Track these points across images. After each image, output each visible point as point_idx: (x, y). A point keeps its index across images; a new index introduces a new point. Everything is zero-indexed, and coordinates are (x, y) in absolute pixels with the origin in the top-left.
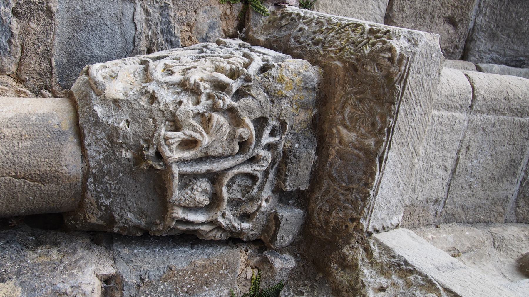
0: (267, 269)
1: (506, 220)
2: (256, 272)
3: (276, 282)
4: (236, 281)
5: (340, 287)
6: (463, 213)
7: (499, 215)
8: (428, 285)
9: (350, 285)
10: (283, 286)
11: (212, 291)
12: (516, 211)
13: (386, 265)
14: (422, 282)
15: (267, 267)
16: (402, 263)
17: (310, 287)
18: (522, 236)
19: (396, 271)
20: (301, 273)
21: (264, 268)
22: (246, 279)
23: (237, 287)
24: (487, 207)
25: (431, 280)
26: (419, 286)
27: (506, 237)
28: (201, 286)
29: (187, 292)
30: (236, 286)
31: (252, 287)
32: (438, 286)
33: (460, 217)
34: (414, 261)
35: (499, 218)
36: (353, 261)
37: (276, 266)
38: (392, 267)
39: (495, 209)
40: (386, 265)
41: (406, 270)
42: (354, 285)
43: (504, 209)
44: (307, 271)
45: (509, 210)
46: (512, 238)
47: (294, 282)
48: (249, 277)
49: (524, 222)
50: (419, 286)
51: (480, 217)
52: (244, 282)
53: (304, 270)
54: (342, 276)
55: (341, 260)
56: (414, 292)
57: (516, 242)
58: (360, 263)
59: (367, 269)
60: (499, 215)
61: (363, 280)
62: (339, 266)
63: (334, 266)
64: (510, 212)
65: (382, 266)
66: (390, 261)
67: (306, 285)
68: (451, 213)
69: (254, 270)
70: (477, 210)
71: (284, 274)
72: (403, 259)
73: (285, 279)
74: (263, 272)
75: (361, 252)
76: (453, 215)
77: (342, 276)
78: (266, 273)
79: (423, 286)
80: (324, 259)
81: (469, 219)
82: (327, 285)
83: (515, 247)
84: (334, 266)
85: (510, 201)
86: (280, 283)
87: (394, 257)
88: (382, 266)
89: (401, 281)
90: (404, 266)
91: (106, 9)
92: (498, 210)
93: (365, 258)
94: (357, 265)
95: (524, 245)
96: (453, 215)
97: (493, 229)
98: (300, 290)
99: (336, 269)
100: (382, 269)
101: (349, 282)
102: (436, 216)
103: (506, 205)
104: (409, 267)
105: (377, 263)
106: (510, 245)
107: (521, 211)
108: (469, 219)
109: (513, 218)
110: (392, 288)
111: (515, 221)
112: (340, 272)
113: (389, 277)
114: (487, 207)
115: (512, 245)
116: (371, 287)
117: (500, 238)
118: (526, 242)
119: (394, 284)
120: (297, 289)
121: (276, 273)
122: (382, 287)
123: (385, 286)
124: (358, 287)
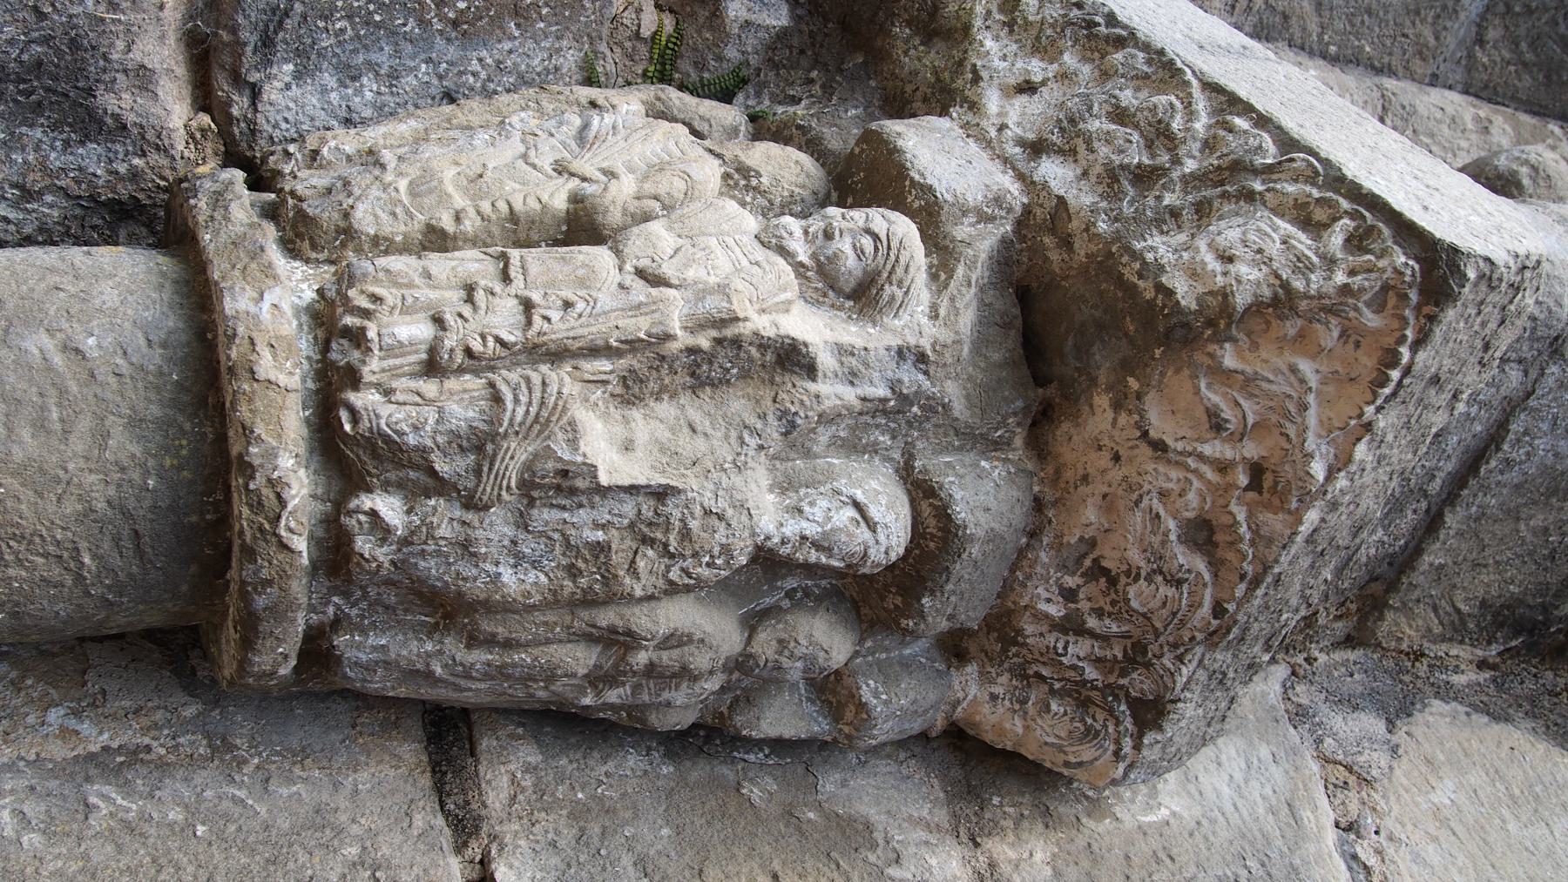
0: (701, 20)
1: (1435, 76)
2: (669, 23)
3: (725, 66)
4: (605, 32)
5: (909, 88)
6: (1316, 19)
7: (1420, 53)
8: (1161, 73)
9: (938, 80)
10: (745, 81)
11: (530, 44)
12: (1471, 56)
13: (1052, 26)
14: (1145, 68)
15: (703, 13)
16: (1098, 19)
17: (823, 87)
18: (1468, 118)
19: (1076, 41)
20: (802, 52)
21: (693, 14)
22: (637, 35)
23: (608, 53)
24: (1390, 17)
25: (1171, 62)
26: (1136, 77)
27: (1421, 109)
28: (499, 16)
29: (455, 24)
30: (603, 47)
31: (652, 69)
32: (1189, 76)
33: (1304, 29)
34: (1136, 19)
35: (1417, 66)
36: (958, 18)
37: (731, 14)
38: (1068, 32)
39: (1410, 32)
40: (1052, 26)
41: (1107, 39)
42: (948, 80)
43: (1437, 38)
44: (822, 46)
45: (1452, 47)
46: (1439, 115)
47: (778, 75)
48: (646, 32)
49: (1484, 94)
50: (1136, 77)
51: (1362, 48)
52: (628, 44)
53: (813, 45)
54: (919, 59)
55: (924, 15)
56: (1117, 92)
57: (1446, 130)
58: (978, 23)
59: (997, 38)
60: (1420, 53)
61: (979, 64)
62: (916, 32)
63: (900, 31)
64: (1454, 53)
65: (1041, 30)
66: (1066, 15)
68: (1280, 8)
69: (663, 16)
70: (1358, 21)
71: (751, 43)
72: (1106, 10)
73: (754, 60)
74: (690, 30)
76: (1286, 17)
77: (919, 59)
78: (699, 33)
79: (1146, 77)
80: (876, 14)
81: (1328, 44)
82: (873, 83)
83: (1439, 144)
85: (1462, 16)
86: (735, 72)
88: (1041, 30)
89: (1086, 70)
90: (1103, 29)
92: (1418, 36)
93: (995, 10)
94: (967, 28)
95: (1464, 144)
96: (1286, 17)
97: (1390, 83)
99: (907, 41)
100: (1038, 38)
101: (935, 72)
102: (1233, 7)
103: (1449, 24)
104: (1118, 31)
105: (1027, 23)
106: (1426, 134)
107: (1485, 60)
108: (1328, 44)
109: (1458, 76)
110: (1055, 86)
111: (1460, 87)
112: (915, 48)
114: (1390, 17)
115: (1432, 135)
116: (996, 81)
117: (1404, 107)
118: (1474, 137)
119: (1064, 76)
120: (783, 91)
121: (728, 35)
122: (1027, 82)
123: (1037, 78)
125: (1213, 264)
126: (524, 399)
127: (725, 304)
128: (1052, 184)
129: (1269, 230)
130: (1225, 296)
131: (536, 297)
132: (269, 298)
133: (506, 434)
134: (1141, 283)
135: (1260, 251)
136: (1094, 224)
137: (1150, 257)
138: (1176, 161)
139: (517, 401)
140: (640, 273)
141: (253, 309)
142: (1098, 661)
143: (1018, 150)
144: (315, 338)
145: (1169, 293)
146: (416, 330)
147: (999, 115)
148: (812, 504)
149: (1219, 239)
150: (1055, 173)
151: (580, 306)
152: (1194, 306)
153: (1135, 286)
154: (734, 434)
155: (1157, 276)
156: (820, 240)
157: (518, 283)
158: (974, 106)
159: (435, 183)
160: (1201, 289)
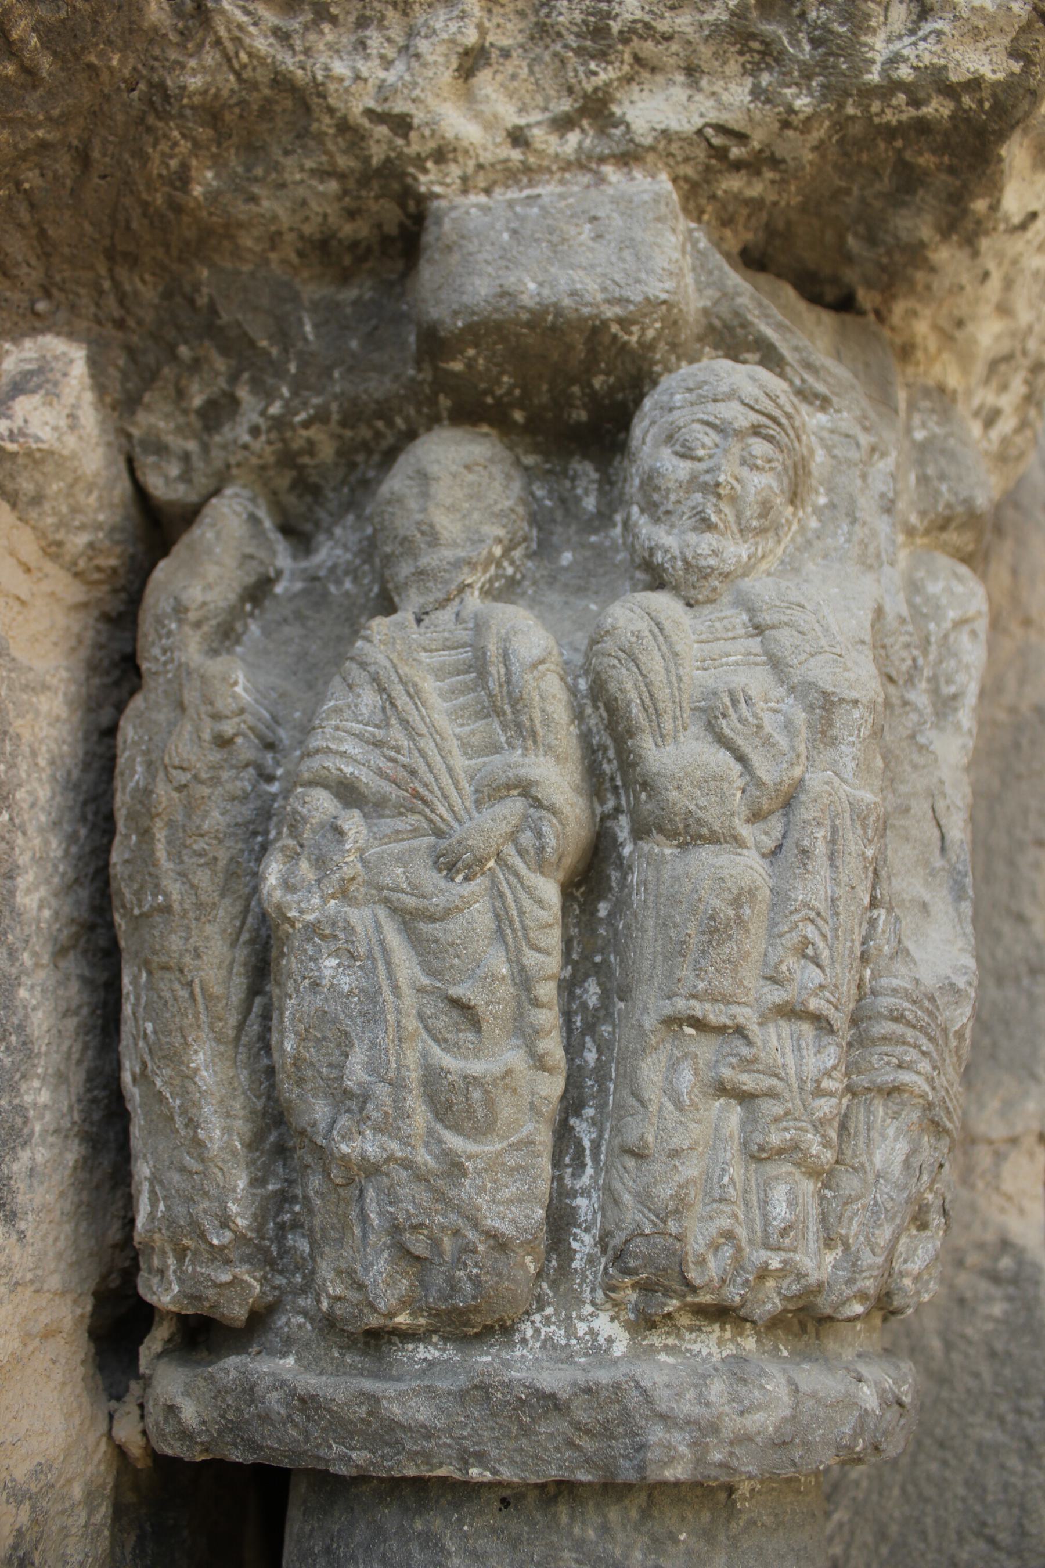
58: (288, 62)
94: (281, 82)
98: (197, 401)
122: (467, 53)
126: (912, 1055)
134: (927, 110)
136: (791, 110)
137: (904, 73)
142: (157, 1423)
143: (573, 138)
144: (691, 1329)
145: (975, 84)
157: (746, 1015)
160: (1004, 41)
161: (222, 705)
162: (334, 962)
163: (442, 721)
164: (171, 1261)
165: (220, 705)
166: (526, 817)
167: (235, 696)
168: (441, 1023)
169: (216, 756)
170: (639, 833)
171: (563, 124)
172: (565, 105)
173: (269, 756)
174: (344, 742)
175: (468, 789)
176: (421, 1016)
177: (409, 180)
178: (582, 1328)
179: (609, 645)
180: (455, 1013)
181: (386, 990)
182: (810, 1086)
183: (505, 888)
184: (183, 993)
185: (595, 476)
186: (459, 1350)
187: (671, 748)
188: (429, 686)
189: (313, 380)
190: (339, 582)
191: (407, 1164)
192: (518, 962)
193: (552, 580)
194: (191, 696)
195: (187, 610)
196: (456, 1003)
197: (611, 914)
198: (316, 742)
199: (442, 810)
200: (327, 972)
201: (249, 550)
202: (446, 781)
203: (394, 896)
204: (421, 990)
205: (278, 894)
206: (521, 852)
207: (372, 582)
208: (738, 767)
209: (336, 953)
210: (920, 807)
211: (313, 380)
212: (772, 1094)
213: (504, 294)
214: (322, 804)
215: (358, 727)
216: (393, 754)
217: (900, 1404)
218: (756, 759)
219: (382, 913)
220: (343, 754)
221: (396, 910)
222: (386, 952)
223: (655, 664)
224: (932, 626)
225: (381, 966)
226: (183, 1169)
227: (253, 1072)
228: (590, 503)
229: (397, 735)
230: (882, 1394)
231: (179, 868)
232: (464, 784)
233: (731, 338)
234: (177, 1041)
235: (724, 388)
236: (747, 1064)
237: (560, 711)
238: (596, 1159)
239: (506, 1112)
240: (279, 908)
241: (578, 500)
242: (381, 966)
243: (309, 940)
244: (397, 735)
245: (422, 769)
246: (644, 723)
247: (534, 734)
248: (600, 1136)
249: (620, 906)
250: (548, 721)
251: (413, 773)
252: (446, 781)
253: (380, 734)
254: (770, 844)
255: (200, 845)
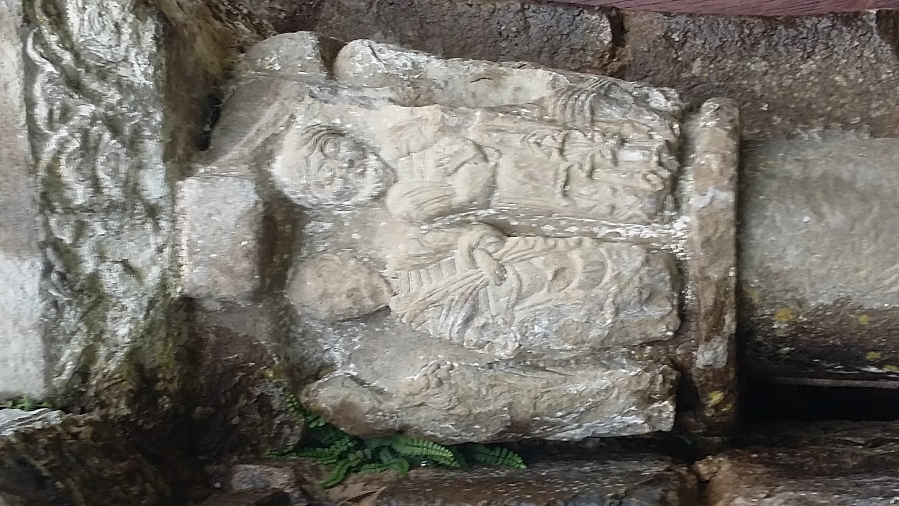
16: (54, 277)
40: (80, 304)
42: (163, 327)
58: (120, 355)
61: (141, 316)
63: (166, 403)
65: (90, 309)
67: (241, 414)
75: (99, 376)
84: (166, 403)
87: (55, 303)
91: (805, 41)
98: (258, 416)
113: (95, 278)
124: (161, 317)
125: (126, 31)
127: (446, 117)
128: (162, 176)
129: (86, 23)
130: (134, 10)
131: (556, 155)
132: (707, 199)
133: (593, 92)
135: (101, 15)
138: (94, 118)
139: (583, 103)
140: (486, 159)
141: (717, 192)
143: (163, 224)
146: (629, 156)
147: (154, 263)
148: (405, 65)
149: (113, 43)
150: (153, 184)
151: (532, 140)
152: (150, 20)
153: (166, 65)
154: (450, 88)
155: (156, 55)
156: (357, 163)
157: (563, 166)
158: (163, 285)
159: (589, 269)
161: (423, 384)
162: (536, 327)
163: (442, 283)
164: (656, 405)
165: (423, 384)
166: (482, 250)
167: (419, 379)
168: (562, 283)
169: (446, 386)
170: (487, 206)
171: (157, 228)
172: (149, 226)
173: (442, 367)
174: (446, 324)
175: (470, 272)
176: (559, 291)
177: (173, 302)
178: (680, 234)
179: (414, 215)
180: (559, 277)
181: (549, 304)
182: (590, 142)
183: (510, 257)
184: (546, 396)
185: (313, 223)
186: (687, 283)
187: (458, 191)
188: (426, 287)
189: (258, 355)
190: (354, 344)
191: (616, 296)
192: (539, 252)
193: (368, 242)
194: (418, 400)
195: (373, 407)
196: (556, 275)
197: (517, 220)
198: (447, 336)
199: (478, 282)
200: (541, 330)
201: (340, 385)
202: (466, 281)
203: (512, 302)
204: (549, 291)
205: (508, 352)
206: (497, 251)
207: (357, 326)
208: (466, 165)
209: (533, 326)
210: (472, 87)
211: (258, 355)
212: (593, 157)
213: (246, 256)
214: (470, 334)
215: (442, 317)
216: (454, 302)
217: (718, 109)
218: (464, 159)
219: (517, 308)
220: (453, 324)
221: (517, 303)
222: (532, 306)
223: (424, 196)
224: (379, 72)
225: (539, 307)
226: (617, 398)
227: (578, 369)
228: (327, 226)
229: (446, 302)
230: (711, 118)
231: (493, 401)
232: (467, 274)
233: (261, 160)
234: (565, 399)
235: (303, 162)
236: (581, 167)
237: (441, 235)
238: (615, 227)
239: (596, 258)
240: (514, 351)
241: (326, 231)
242: (539, 307)
243: (527, 337)
244: (446, 302)
245: (461, 290)
246: (446, 202)
247: (448, 246)
248: (605, 225)
249: (514, 214)
250: (444, 240)
251: (463, 294)
252: (466, 281)
253: (446, 308)
254: (497, 155)
255: (484, 391)
